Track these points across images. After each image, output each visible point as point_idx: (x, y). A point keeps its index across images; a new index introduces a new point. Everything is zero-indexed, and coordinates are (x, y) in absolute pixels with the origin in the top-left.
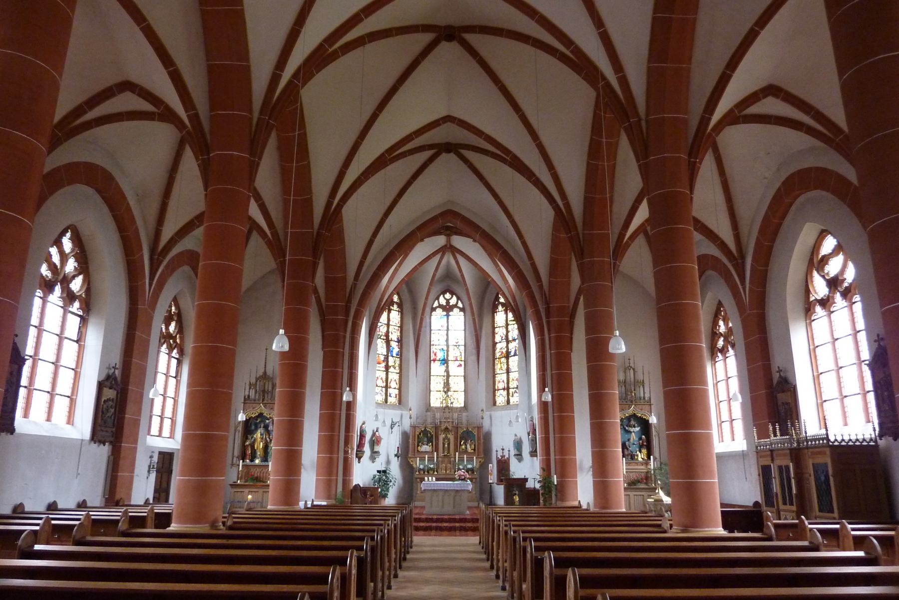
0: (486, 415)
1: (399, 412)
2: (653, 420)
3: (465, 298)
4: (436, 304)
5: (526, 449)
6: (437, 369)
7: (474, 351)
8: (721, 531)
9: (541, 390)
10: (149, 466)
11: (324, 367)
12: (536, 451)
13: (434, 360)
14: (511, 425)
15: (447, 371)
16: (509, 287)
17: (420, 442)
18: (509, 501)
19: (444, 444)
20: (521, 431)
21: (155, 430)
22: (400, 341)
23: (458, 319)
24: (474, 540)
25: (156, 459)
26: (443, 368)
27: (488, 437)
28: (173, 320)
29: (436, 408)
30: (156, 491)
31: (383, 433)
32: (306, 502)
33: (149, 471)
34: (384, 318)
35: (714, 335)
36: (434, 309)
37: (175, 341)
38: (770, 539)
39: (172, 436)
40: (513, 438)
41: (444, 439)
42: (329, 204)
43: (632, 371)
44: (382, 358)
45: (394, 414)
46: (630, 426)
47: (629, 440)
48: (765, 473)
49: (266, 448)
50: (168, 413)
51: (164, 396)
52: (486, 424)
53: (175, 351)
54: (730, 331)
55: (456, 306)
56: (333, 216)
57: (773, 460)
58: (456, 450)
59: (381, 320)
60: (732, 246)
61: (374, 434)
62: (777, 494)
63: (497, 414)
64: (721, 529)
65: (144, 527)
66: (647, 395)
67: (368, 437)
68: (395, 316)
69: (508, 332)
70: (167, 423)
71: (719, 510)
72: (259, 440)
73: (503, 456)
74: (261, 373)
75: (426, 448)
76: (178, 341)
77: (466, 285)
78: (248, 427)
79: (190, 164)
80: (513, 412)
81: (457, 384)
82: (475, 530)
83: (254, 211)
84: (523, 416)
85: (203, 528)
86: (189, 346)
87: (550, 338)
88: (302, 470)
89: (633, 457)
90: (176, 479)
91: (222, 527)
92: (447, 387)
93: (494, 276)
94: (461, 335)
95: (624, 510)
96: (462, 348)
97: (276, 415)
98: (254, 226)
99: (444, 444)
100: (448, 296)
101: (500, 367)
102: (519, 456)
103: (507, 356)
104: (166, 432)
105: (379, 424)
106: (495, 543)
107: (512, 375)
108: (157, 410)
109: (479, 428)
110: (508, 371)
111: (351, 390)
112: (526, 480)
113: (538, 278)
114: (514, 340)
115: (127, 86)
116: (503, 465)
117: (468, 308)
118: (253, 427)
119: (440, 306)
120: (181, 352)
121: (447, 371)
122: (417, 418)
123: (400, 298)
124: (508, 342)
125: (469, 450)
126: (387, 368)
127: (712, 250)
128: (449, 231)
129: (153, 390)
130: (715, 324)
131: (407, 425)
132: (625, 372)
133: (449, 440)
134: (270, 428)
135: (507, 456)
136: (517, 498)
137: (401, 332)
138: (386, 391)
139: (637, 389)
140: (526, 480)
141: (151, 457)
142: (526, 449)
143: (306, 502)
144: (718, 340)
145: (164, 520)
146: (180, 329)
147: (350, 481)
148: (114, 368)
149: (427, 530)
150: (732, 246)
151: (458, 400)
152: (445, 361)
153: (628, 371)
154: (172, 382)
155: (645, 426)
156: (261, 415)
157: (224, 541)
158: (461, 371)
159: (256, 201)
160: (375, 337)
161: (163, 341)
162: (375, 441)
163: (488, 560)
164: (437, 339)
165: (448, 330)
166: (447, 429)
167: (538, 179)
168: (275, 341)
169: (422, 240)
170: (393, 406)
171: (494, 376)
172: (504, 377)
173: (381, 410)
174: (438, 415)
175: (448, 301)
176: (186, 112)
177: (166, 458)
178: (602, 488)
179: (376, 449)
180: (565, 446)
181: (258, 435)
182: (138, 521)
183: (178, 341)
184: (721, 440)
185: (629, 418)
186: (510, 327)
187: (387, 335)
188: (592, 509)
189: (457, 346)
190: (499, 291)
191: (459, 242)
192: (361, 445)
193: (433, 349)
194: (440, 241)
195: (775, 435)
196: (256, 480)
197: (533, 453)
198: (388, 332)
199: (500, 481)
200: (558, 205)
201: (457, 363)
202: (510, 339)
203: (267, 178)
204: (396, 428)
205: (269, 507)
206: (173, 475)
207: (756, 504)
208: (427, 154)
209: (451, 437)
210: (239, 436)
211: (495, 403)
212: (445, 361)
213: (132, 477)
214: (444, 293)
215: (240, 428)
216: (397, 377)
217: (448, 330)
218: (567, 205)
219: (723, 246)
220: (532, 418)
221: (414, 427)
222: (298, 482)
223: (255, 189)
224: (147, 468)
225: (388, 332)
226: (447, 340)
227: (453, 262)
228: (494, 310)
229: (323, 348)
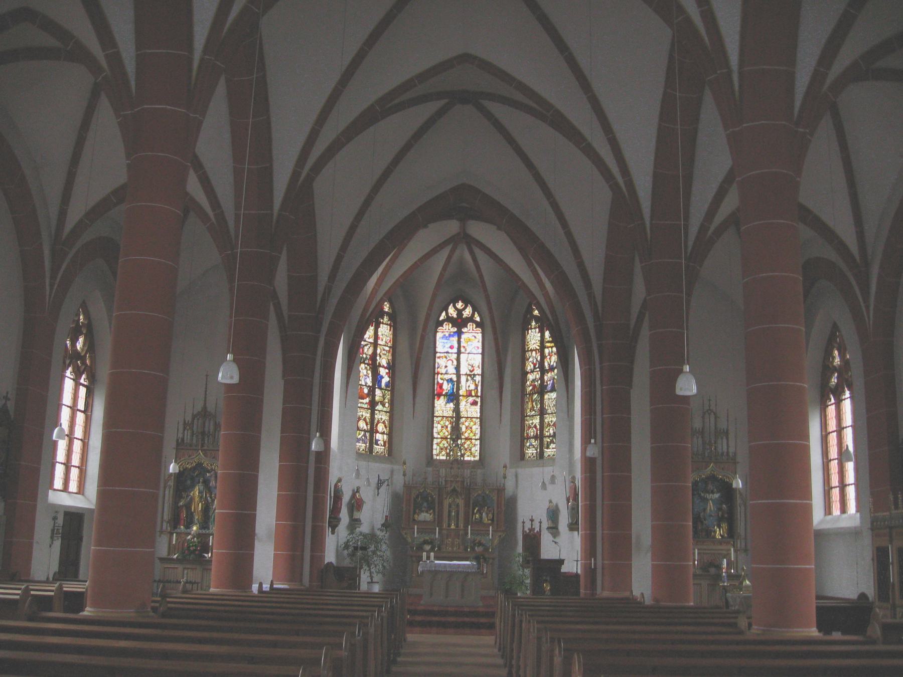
0: (510, 473)
1: (388, 466)
2: (738, 483)
3: (484, 308)
4: (443, 316)
5: (564, 520)
6: (442, 407)
7: (496, 384)
8: (813, 632)
9: (586, 442)
10: (53, 531)
11: (284, 402)
12: (577, 523)
13: (439, 395)
14: (546, 490)
15: (457, 410)
16: (546, 294)
17: (418, 508)
18: (537, 589)
19: (450, 512)
20: (559, 495)
21: (58, 483)
22: (391, 367)
23: (473, 339)
24: (489, 639)
25: (60, 521)
26: (451, 405)
27: (511, 503)
28: (81, 334)
29: (441, 461)
30: (62, 563)
31: (366, 494)
32: (261, 585)
33: (52, 537)
34: (369, 334)
35: (827, 369)
36: (441, 324)
37: (84, 363)
38: (874, 642)
39: (81, 490)
40: (547, 505)
41: (450, 506)
42: (295, 175)
43: (712, 415)
44: (366, 391)
45: (381, 469)
46: (708, 492)
47: (705, 510)
48: (881, 558)
49: (207, 509)
50: (76, 460)
51: (71, 438)
52: (510, 484)
53: (84, 376)
54: (846, 363)
55: (471, 319)
56: (302, 191)
57: (891, 542)
58: (467, 522)
59: (366, 336)
60: (854, 248)
61: (353, 496)
62: (893, 584)
63: (524, 472)
64: (815, 629)
65: (51, 610)
66: (731, 450)
67: (346, 498)
68: (385, 331)
69: (543, 357)
70: (74, 473)
71: (813, 604)
72: (197, 499)
73: (532, 529)
74: (199, 407)
75: (425, 516)
76: (88, 362)
77: (485, 290)
78: (183, 482)
79: (106, 119)
80: (548, 471)
81: (472, 429)
82: (491, 627)
83: (194, 187)
84: (562, 475)
85: (128, 614)
86: (104, 371)
87: (601, 369)
88: (257, 544)
89: (709, 533)
90: (89, 549)
91: (152, 614)
92: (456, 433)
93: (526, 276)
94: (477, 360)
95: (692, 604)
96: (478, 378)
97: (220, 467)
98: (190, 206)
99: (450, 512)
100: (460, 305)
101: (531, 409)
102: (554, 529)
103: (542, 390)
104: (73, 487)
105: (357, 483)
106: (515, 645)
107: (548, 419)
108: (61, 456)
109: (501, 490)
110: (542, 413)
111: (321, 436)
112: (561, 562)
113: (588, 284)
114: (552, 369)
115: (26, 15)
116: (533, 541)
117: (488, 322)
118: (189, 482)
119: (449, 319)
120: (92, 378)
121: (457, 410)
122: (414, 475)
123: (392, 306)
124: (543, 371)
125: (485, 520)
126: (373, 405)
127: (831, 254)
128: (465, 215)
129: (56, 430)
130: (828, 354)
131: (399, 482)
132: (703, 417)
133: (458, 505)
134: (212, 483)
135: (537, 529)
136: (547, 587)
137: (393, 355)
138: (372, 436)
139: (719, 441)
140: (561, 562)
141: (55, 518)
142: (564, 520)
143: (261, 585)
144: (830, 377)
145: (75, 601)
146: (91, 345)
147: (322, 558)
148: (6, 398)
149: (426, 626)
150: (854, 248)
151: (472, 453)
152: (453, 397)
153: (707, 416)
154: (80, 418)
155: (728, 492)
156: (199, 465)
157: (158, 632)
158: (475, 411)
159: (196, 172)
160: (357, 361)
161: (68, 362)
162: (356, 504)
163: (505, 666)
164: (445, 366)
165: (459, 353)
166: (454, 490)
167: (589, 145)
168: (222, 369)
169: (425, 226)
170: (379, 458)
171: (523, 417)
172: (537, 421)
173: (363, 464)
174: (443, 472)
175: (460, 312)
176: (104, 51)
177: (74, 519)
178: (668, 574)
179: (356, 515)
180: (620, 517)
181: (196, 492)
182: (44, 603)
183: (88, 362)
184: (828, 510)
185: (705, 481)
186: (547, 351)
187: (374, 356)
188: (648, 601)
189: (472, 376)
190: (533, 300)
191: (479, 230)
192: (336, 510)
193: (439, 379)
194: (452, 227)
195: (897, 508)
196: (195, 555)
197: (573, 527)
198: (374, 354)
199: (526, 563)
200: (617, 184)
201: (471, 399)
202: (547, 368)
203: (214, 144)
204: (383, 489)
205: (212, 590)
206: (84, 543)
207: (863, 596)
208: (433, 107)
209: (461, 502)
210: (169, 494)
211: (522, 456)
212: (453, 397)
213: (31, 546)
214: (454, 302)
215: (171, 483)
216: (385, 417)
217: (459, 353)
218: (630, 184)
219: (841, 247)
220: (574, 478)
221: (408, 487)
222: (251, 557)
223: (196, 157)
224: (49, 534)
225: (374, 354)
226: (458, 368)
227: (468, 257)
228: (525, 328)
229: (284, 376)
